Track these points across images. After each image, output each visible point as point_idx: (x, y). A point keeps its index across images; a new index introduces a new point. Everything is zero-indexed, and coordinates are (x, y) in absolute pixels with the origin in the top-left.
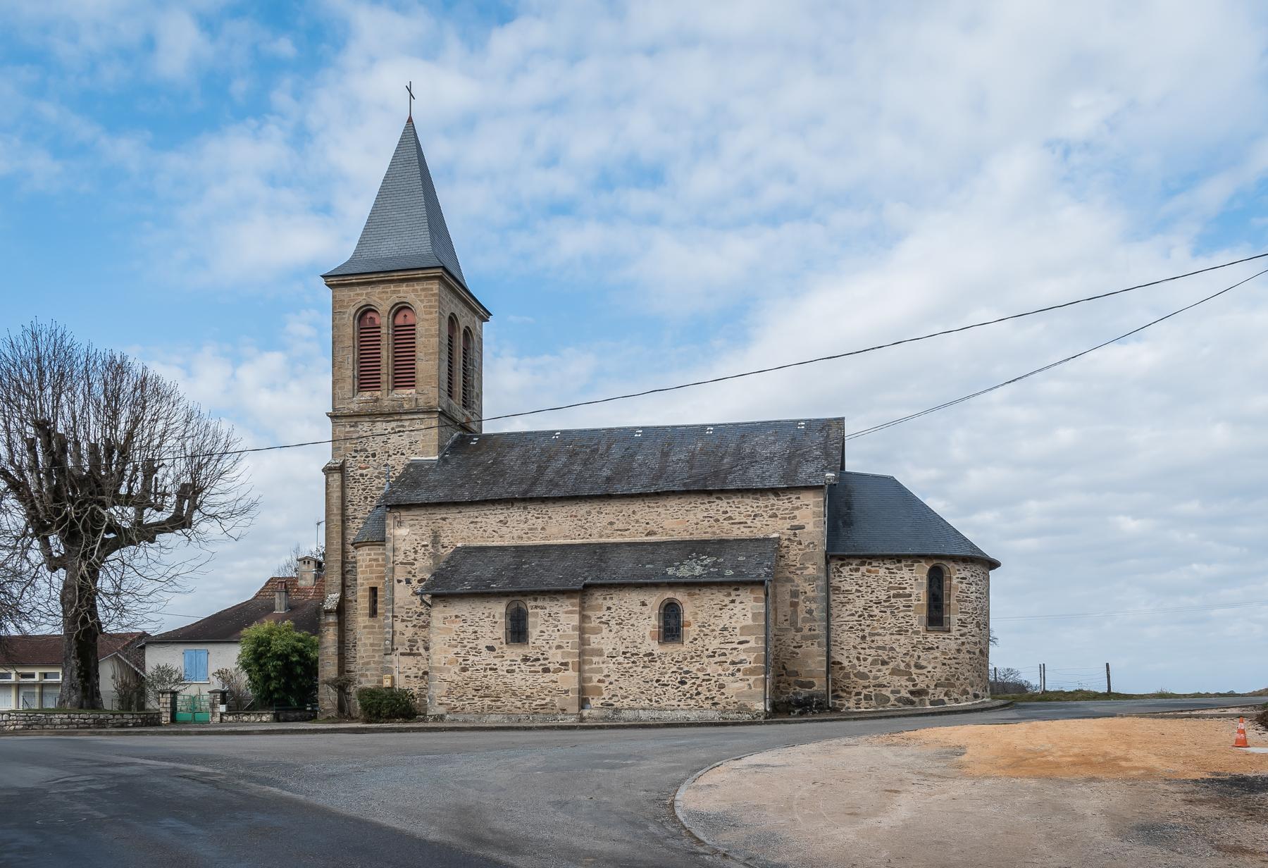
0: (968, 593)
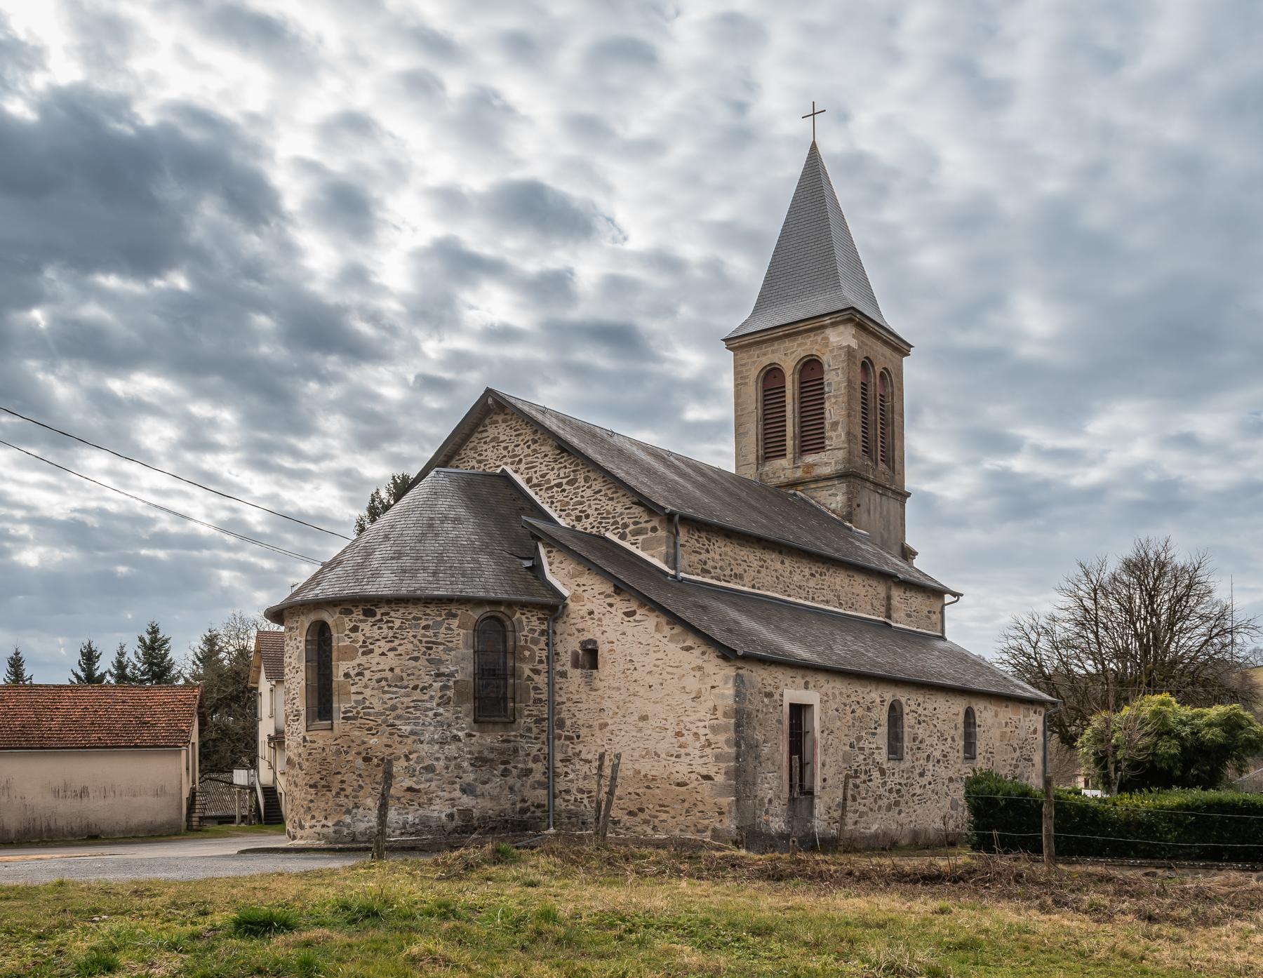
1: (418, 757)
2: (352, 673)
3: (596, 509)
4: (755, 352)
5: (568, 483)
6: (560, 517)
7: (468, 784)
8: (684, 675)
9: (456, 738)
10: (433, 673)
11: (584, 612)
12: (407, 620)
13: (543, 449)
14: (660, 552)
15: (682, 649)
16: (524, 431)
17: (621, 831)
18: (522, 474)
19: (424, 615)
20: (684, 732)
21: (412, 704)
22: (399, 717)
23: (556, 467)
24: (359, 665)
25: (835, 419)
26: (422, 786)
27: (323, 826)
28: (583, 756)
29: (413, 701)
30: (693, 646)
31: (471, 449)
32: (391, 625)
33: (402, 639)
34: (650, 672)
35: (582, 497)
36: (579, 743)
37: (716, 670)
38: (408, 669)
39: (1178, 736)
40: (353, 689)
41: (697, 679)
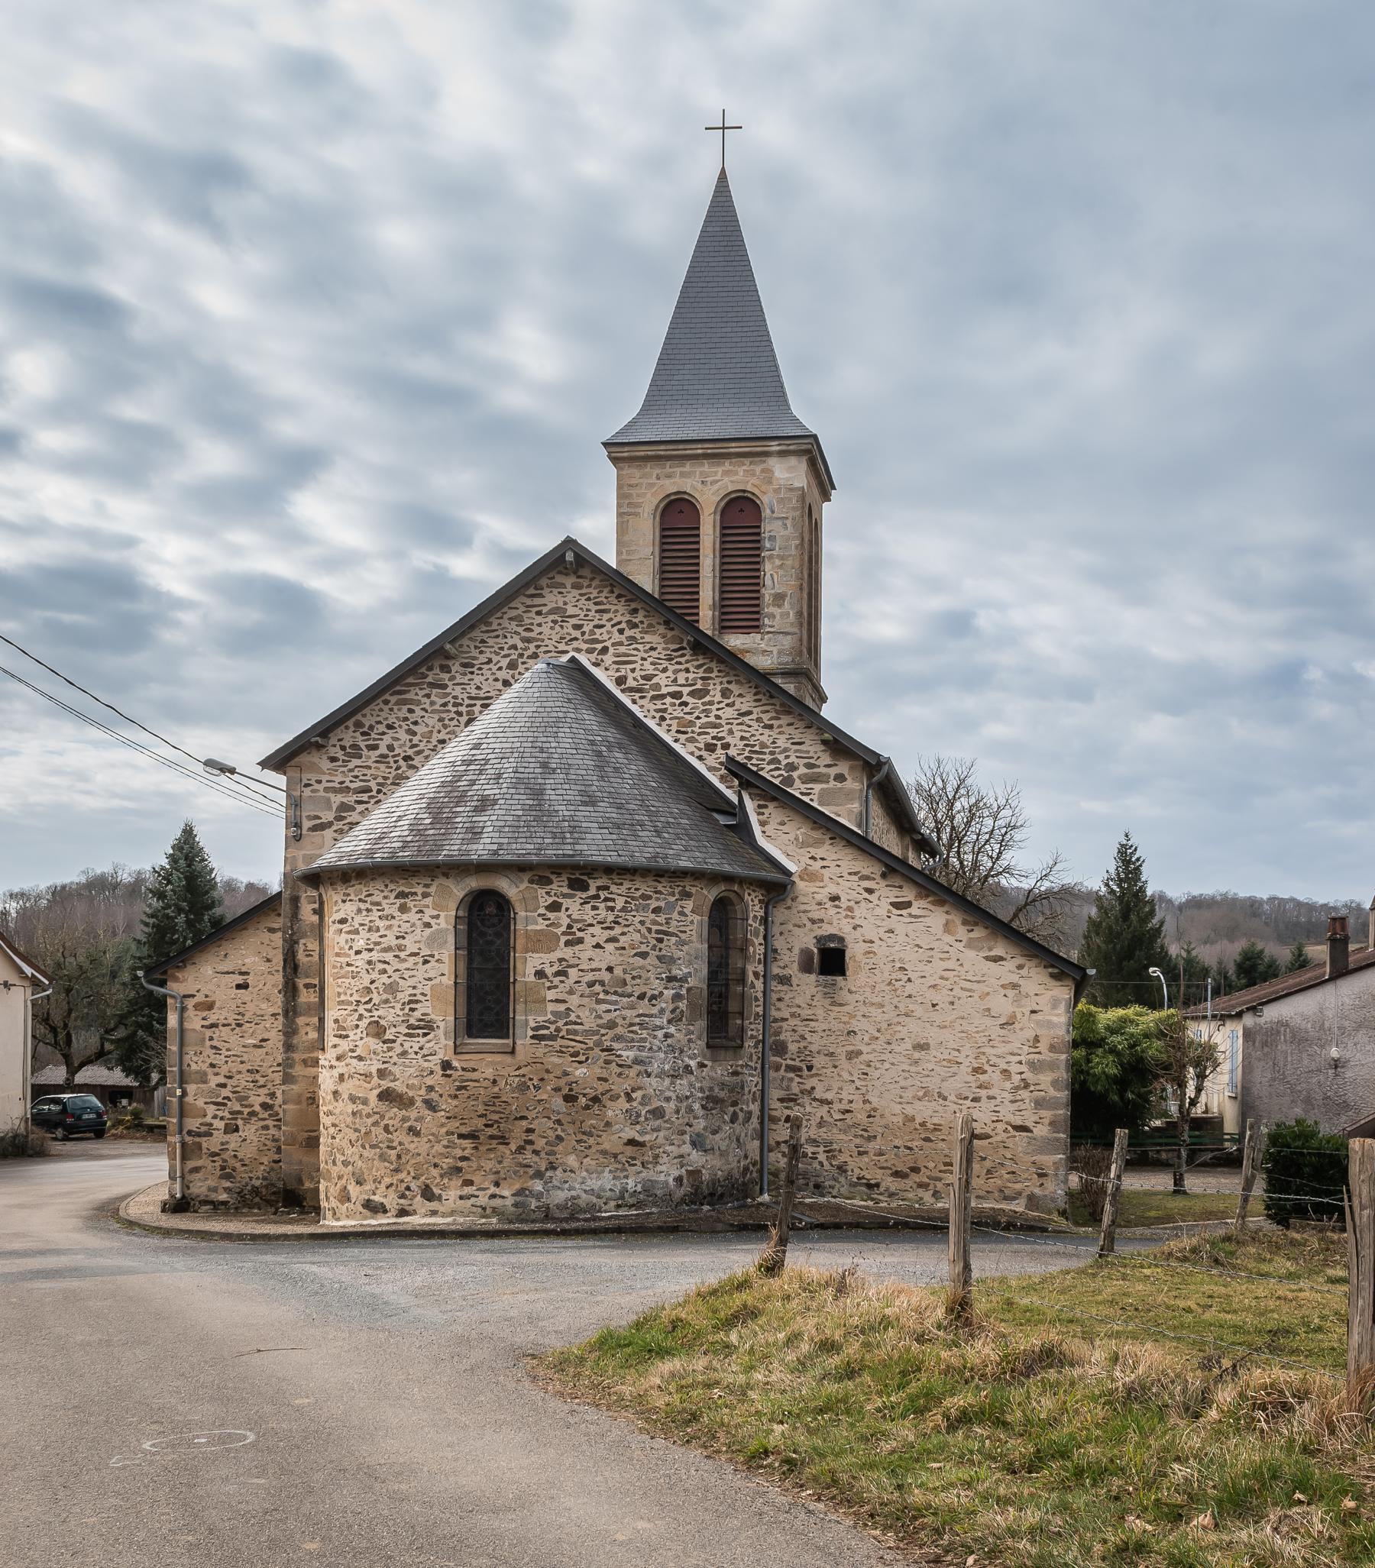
0: (349, 956)
1: (644, 1096)
2: (549, 971)
3: (742, 738)
4: (653, 471)
5: (691, 694)
6: (676, 741)
7: (698, 1135)
8: (988, 994)
9: (688, 1069)
10: (664, 976)
11: (823, 895)
12: (633, 898)
13: (648, 638)
14: (850, 811)
15: (987, 958)
16: (613, 608)
17: (881, 1197)
18: (607, 669)
19: (656, 892)
20: (986, 1067)
21: (637, 1020)
22: (618, 1038)
23: (671, 668)
24: (561, 960)
25: (779, 589)
26: (647, 1138)
27: (493, 1196)
28: (818, 1094)
29: (639, 1016)
30: (1004, 955)
31: (511, 619)
32: (610, 904)
33: (626, 926)
34: (934, 986)
35: (718, 717)
36: (812, 1076)
37: (1040, 989)
38: (633, 969)
39: (1113, 1051)
40: (551, 995)
41: (1010, 1000)
